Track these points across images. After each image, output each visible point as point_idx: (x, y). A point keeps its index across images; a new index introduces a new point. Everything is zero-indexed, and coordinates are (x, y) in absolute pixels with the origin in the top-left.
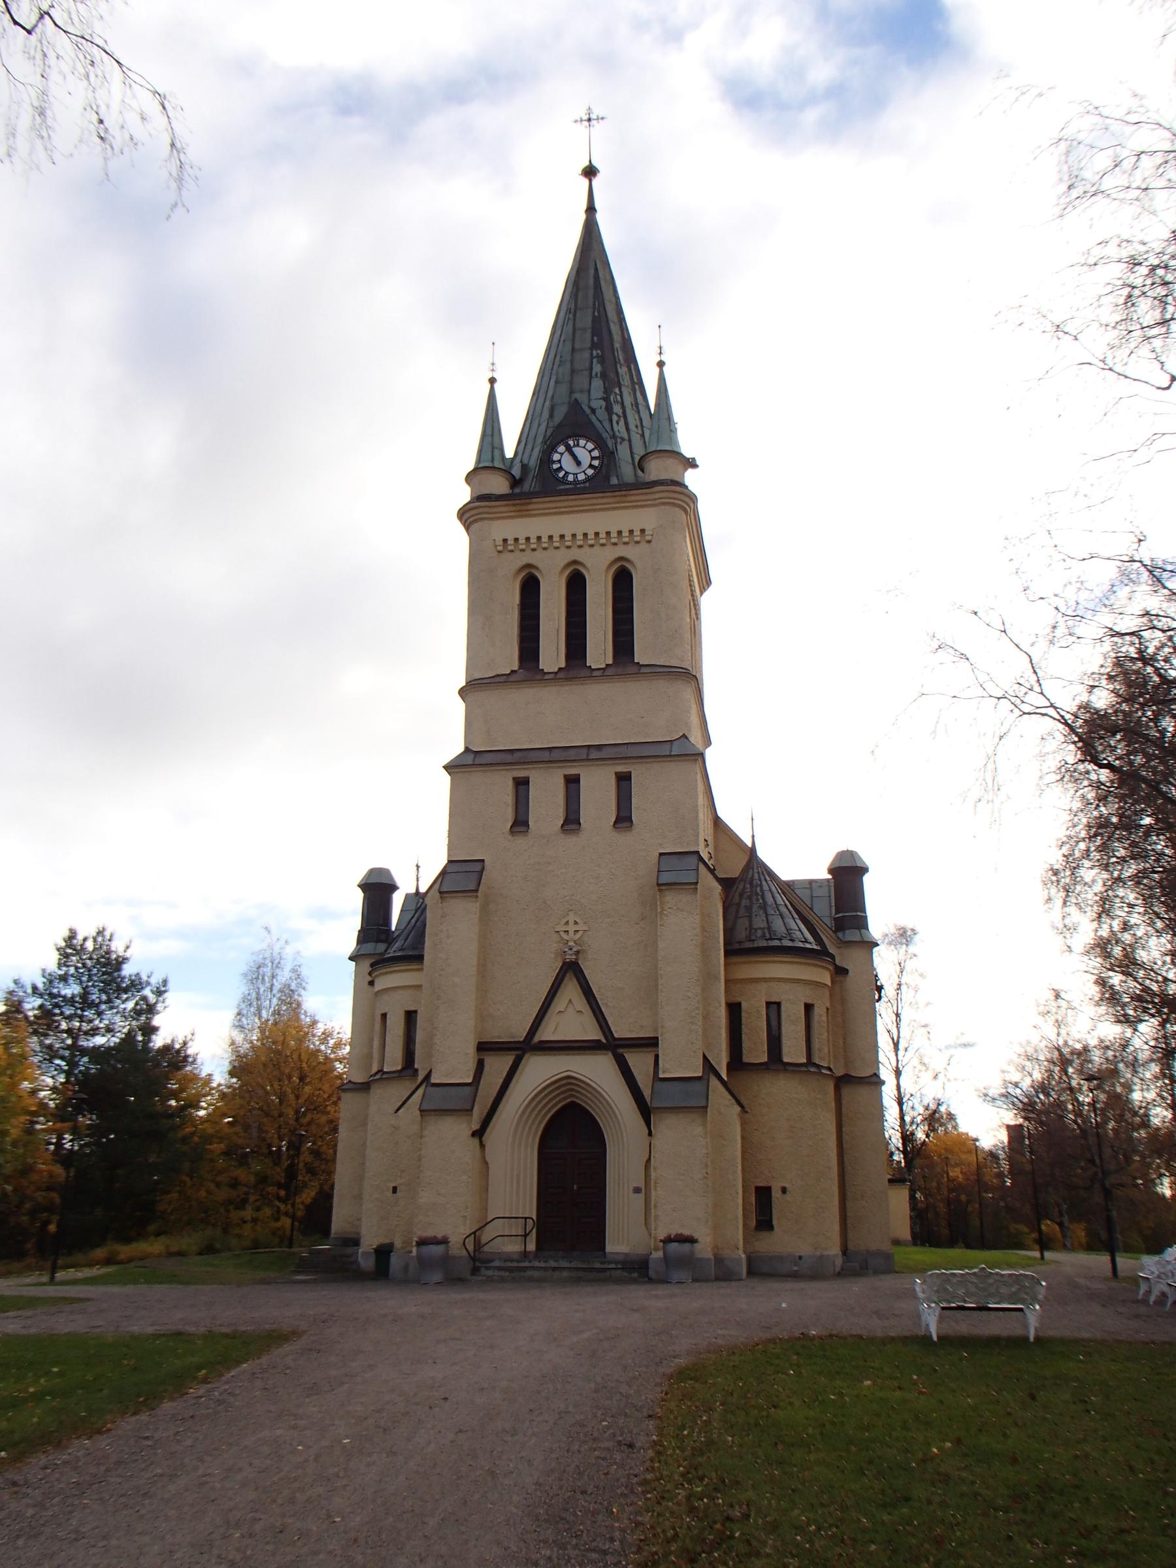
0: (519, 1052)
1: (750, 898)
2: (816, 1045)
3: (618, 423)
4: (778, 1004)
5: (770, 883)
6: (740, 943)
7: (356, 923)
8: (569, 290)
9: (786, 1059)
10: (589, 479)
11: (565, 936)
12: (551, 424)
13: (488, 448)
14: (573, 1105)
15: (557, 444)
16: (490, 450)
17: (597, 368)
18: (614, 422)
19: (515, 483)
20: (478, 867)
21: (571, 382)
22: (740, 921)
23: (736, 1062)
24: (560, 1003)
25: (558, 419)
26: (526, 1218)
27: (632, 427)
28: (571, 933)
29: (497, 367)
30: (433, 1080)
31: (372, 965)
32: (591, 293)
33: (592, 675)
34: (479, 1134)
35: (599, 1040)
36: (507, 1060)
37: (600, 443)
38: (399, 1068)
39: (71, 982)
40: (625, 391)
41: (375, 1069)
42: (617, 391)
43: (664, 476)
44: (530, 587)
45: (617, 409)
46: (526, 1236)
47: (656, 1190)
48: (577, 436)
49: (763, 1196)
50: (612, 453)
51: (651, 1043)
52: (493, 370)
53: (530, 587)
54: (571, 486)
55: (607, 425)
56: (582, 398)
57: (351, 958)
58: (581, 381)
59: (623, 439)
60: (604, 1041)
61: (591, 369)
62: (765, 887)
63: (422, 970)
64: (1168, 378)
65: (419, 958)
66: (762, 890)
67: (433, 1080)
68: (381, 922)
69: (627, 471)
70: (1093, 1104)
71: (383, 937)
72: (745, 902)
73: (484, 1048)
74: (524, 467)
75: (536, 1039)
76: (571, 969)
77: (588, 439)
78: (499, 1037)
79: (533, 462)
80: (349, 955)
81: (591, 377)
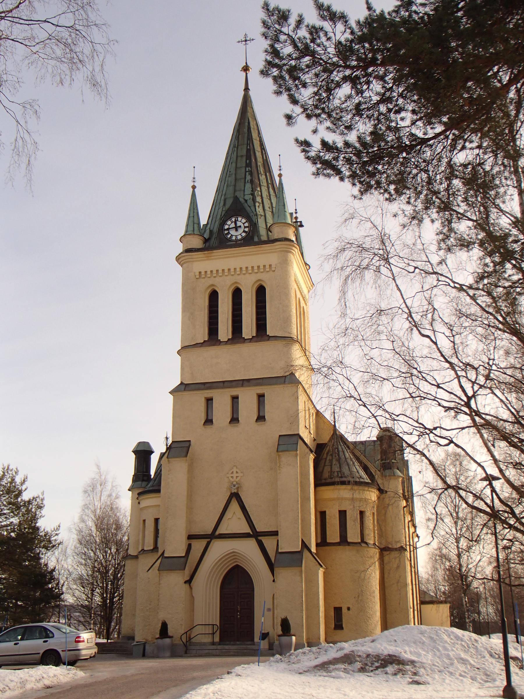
0: (209, 540)
1: (332, 455)
2: (366, 532)
3: (259, 206)
4: (345, 511)
5: (343, 447)
6: (325, 479)
7: (131, 472)
8: (235, 134)
9: (349, 540)
10: (243, 239)
11: (231, 479)
12: (224, 209)
13: (191, 224)
14: (237, 566)
15: (227, 220)
16: (192, 224)
17: (248, 178)
18: (257, 207)
19: (206, 241)
20: (188, 444)
21: (235, 186)
22: (326, 468)
23: (322, 543)
24: (229, 514)
25: (228, 206)
26: (213, 625)
27: (267, 208)
28: (235, 478)
29: (196, 179)
30: (166, 555)
31: (139, 494)
32: (246, 135)
34: (189, 582)
35: (249, 533)
36: (204, 542)
37: (249, 219)
38: (152, 548)
39: (269, 48)
40: (264, 189)
41: (140, 549)
42: (259, 189)
43: (281, 236)
44: (214, 296)
45: (258, 199)
46: (213, 634)
47: (277, 610)
48: (237, 215)
49: (338, 611)
50: (255, 224)
51: (275, 533)
52: (194, 181)
53: (214, 296)
54: (234, 242)
55: (253, 208)
56: (239, 194)
57: (129, 490)
58: (240, 184)
59: (261, 216)
60: (251, 533)
61: (245, 178)
62: (340, 449)
63: (160, 497)
64: (413, 268)
65: (159, 491)
66: (338, 451)
67: (166, 555)
68: (145, 470)
69: (263, 231)
71: (145, 478)
72: (329, 457)
73: (190, 537)
74: (211, 232)
75: (217, 533)
76: (235, 496)
77: (243, 217)
78: (199, 532)
79: (215, 230)
80: (128, 488)
81: (245, 183)
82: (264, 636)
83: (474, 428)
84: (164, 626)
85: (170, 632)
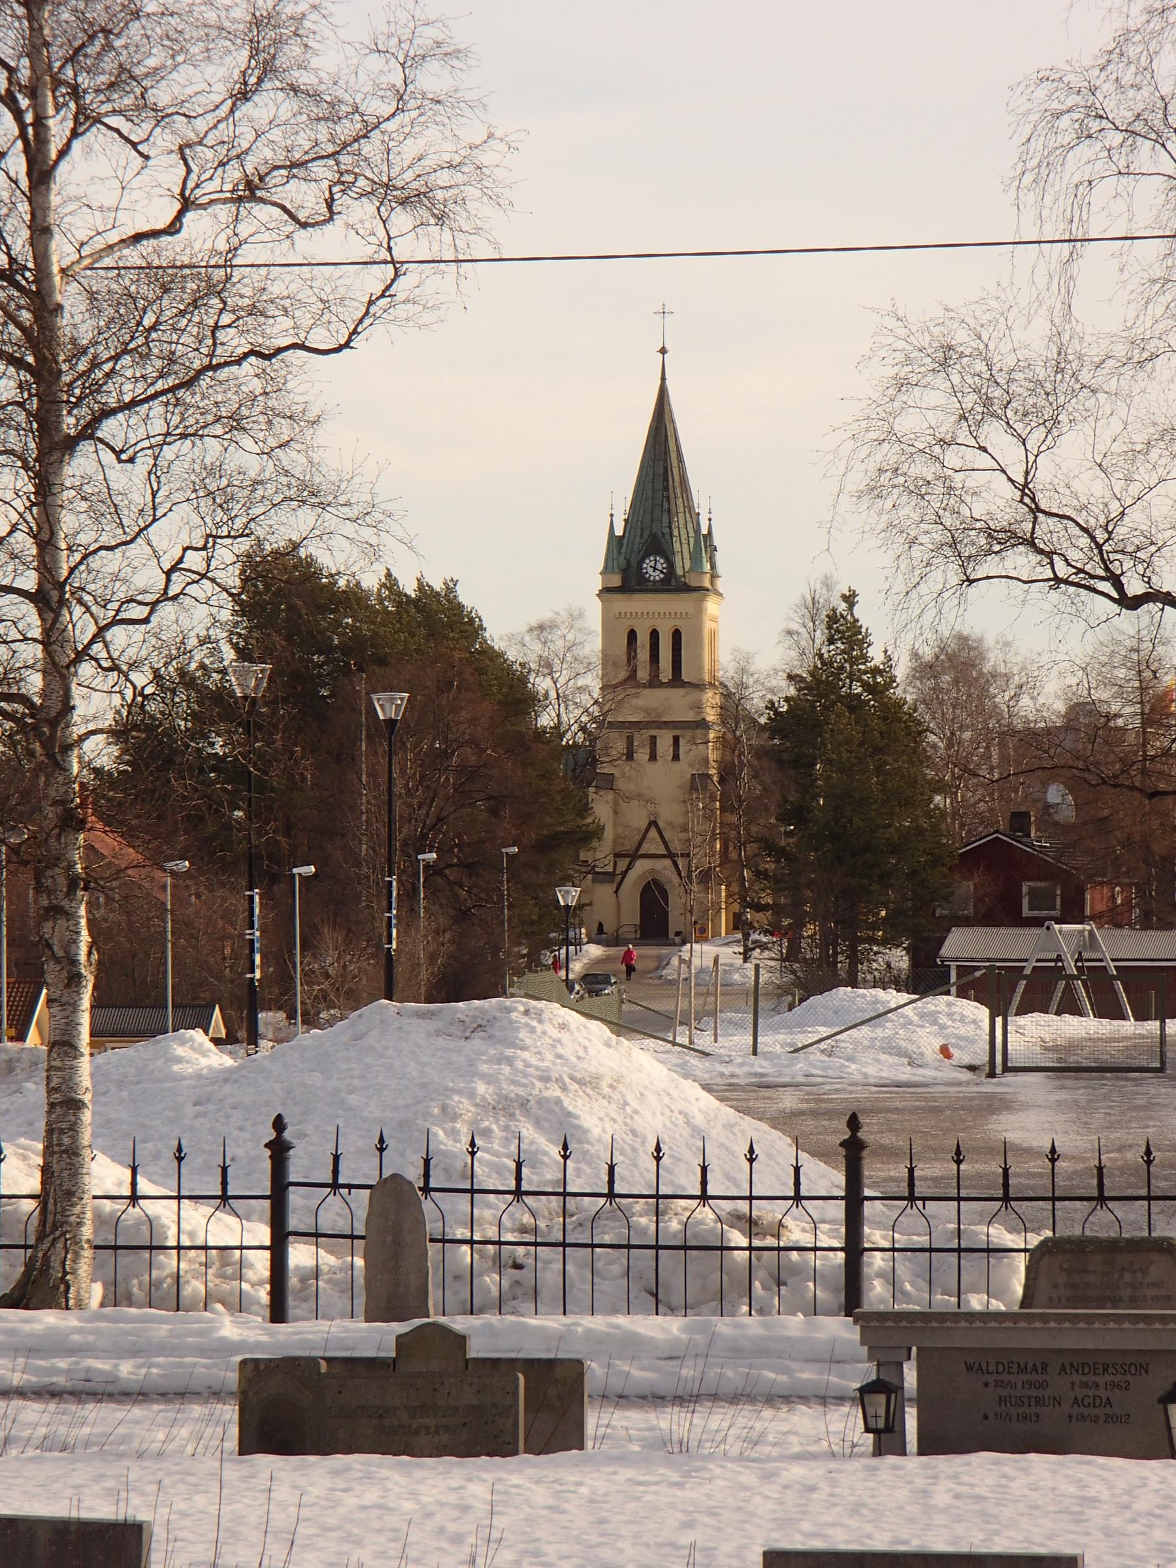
10: (661, 580)
33: (662, 685)
34: (616, 892)
36: (627, 860)
40: (681, 516)
44: (632, 635)
45: (676, 533)
48: (655, 554)
53: (632, 635)
70: (337, 623)
76: (653, 823)
82: (678, 934)
83: (41, 647)
84: (600, 925)
85: (605, 929)
